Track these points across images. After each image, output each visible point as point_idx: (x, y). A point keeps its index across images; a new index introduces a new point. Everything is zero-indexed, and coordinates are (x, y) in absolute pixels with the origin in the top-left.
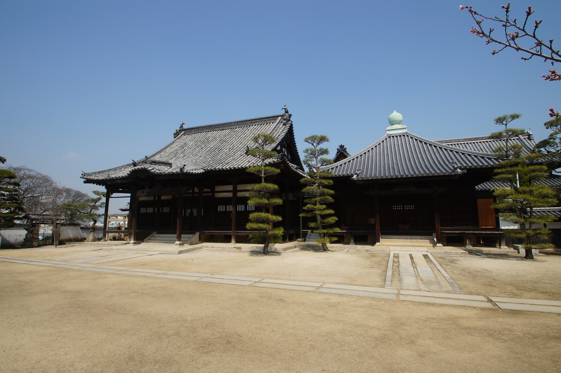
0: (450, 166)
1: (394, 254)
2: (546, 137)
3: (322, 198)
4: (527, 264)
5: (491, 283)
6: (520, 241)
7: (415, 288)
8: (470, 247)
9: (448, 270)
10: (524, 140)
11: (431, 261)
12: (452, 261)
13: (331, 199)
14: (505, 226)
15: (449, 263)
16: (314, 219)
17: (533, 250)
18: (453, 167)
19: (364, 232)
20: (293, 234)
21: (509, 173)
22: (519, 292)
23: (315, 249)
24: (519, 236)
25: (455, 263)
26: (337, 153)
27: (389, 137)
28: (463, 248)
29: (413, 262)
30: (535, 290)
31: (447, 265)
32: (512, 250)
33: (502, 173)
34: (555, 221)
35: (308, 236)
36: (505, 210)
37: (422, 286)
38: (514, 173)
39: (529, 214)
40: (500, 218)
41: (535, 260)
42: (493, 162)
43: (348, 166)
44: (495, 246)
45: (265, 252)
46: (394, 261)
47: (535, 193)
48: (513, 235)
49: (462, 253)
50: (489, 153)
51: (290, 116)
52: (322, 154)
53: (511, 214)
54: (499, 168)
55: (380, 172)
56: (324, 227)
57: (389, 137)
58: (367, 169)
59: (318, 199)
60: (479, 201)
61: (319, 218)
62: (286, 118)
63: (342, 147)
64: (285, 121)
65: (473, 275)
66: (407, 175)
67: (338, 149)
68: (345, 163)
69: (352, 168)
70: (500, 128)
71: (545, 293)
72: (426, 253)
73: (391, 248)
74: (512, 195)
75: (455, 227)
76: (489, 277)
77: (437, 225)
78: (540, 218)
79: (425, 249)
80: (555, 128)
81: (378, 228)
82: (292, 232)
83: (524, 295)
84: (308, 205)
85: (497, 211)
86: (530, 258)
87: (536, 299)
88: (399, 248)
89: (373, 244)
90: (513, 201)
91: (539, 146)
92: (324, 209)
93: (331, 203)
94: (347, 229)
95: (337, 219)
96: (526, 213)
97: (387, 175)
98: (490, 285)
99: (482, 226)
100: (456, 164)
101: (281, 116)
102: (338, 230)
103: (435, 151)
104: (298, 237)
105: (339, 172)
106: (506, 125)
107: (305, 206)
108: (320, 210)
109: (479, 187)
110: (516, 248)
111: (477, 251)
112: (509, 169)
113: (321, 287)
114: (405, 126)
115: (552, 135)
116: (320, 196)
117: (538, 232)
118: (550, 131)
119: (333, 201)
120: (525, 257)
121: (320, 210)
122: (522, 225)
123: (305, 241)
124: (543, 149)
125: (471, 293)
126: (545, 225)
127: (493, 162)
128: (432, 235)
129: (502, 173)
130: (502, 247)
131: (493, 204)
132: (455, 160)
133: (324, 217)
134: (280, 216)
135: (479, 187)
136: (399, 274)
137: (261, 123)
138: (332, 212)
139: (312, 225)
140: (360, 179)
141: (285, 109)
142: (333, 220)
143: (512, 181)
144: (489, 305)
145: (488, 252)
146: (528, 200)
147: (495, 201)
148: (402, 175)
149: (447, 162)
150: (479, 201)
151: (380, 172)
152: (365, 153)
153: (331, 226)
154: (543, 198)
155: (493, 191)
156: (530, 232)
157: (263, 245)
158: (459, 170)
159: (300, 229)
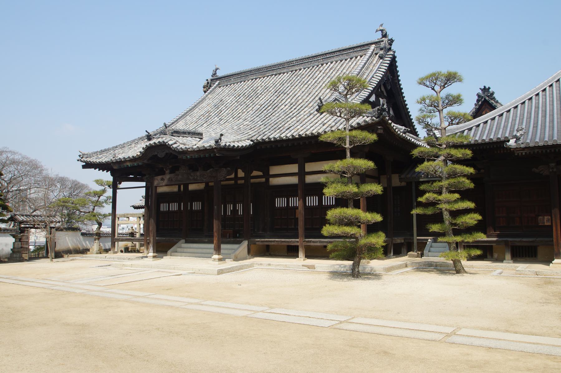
3: (452, 181)
13: (468, 184)
16: (438, 218)
19: (531, 239)
20: (402, 244)
23: (441, 269)
26: (478, 101)
35: (427, 247)
43: (499, 125)
45: (355, 274)
51: (391, 41)
52: (451, 105)
56: (457, 232)
58: (535, 127)
59: (445, 183)
61: (446, 216)
62: (385, 46)
63: (485, 90)
64: (382, 52)
67: (478, 95)
69: (505, 127)
84: (427, 195)
89: (548, 261)
92: (456, 201)
93: (469, 190)
94: (498, 236)
95: (480, 218)
101: (375, 43)
102: (481, 237)
108: (449, 202)
113: (454, 333)
119: (472, 186)
121: (449, 202)
123: (422, 255)
133: (455, 214)
134: (378, 213)
138: (470, 205)
140: (522, 146)
141: (382, 31)
142: (472, 219)
153: (469, 230)
157: (351, 263)
159: (413, 235)
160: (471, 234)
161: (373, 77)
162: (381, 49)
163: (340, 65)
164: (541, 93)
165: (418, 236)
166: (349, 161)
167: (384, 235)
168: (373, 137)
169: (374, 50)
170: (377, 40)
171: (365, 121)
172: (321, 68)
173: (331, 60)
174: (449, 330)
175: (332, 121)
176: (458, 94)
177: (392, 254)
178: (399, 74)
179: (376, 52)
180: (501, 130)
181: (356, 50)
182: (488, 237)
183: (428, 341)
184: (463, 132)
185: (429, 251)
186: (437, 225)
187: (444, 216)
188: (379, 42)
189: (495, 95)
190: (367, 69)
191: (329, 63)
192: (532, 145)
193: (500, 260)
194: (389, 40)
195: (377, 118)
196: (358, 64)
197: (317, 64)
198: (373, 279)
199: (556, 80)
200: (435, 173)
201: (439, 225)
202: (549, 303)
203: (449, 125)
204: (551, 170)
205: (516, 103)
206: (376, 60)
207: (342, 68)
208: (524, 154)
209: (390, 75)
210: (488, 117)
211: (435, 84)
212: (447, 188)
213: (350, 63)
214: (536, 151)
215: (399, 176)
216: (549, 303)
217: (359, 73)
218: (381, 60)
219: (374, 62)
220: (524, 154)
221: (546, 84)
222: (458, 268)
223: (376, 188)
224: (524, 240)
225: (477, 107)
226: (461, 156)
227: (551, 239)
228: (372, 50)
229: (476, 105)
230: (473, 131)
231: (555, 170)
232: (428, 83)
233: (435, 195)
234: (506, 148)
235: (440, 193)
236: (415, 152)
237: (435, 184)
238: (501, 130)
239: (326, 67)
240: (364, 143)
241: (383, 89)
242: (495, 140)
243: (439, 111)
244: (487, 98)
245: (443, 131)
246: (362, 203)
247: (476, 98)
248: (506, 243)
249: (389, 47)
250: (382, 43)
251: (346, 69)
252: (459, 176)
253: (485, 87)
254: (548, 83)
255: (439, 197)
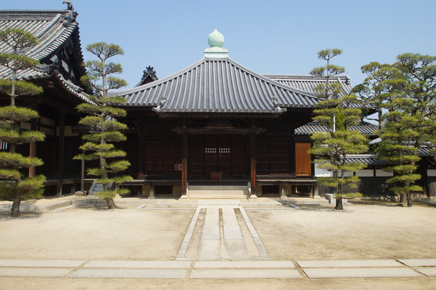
0: (271, 103)
1: (202, 209)
2: (361, 82)
3: (109, 133)
4: (338, 214)
5: (301, 241)
6: (332, 190)
7: (216, 257)
8: (284, 198)
9: (259, 228)
10: (342, 84)
11: (242, 217)
12: (264, 216)
13: (122, 137)
14: (320, 173)
15: (261, 219)
16: (96, 163)
17: (343, 200)
18: (274, 103)
19: (168, 181)
20: (71, 185)
21: (327, 114)
22: (328, 251)
23: (97, 205)
24: (332, 185)
25: (268, 218)
26: (144, 76)
27: (207, 62)
28: (278, 199)
29: (221, 219)
30: (343, 247)
31: (259, 221)
32: (324, 199)
33: (320, 114)
34: (365, 169)
35: (92, 188)
36: (320, 156)
37: (224, 254)
38: (331, 115)
39: (342, 161)
40: (316, 165)
41: (345, 211)
42: (313, 102)
43: (152, 93)
44: (308, 196)
45: (15, 213)
46: (198, 219)
47: (349, 138)
48: (326, 184)
49: (276, 205)
50: (309, 91)
51: (76, 15)
52: (113, 72)
53: (326, 160)
54: (318, 109)
55: (191, 103)
56: (111, 176)
57: (207, 62)
58: (176, 99)
59: (103, 135)
60: (297, 145)
61: (103, 162)
62: (70, 17)
63: (150, 69)
64: (66, 21)
65: (282, 232)
66: (223, 110)
67: (145, 72)
68: (148, 89)
69: (156, 96)
70: (322, 63)
71: (353, 250)
72: (237, 207)
73: (199, 202)
74: (328, 139)
75: (272, 175)
76: (299, 234)
77: (253, 172)
78: (352, 165)
79: (238, 202)
80: (370, 73)
81: (184, 175)
82: (68, 182)
83: (333, 255)
84: (87, 144)
85: (313, 157)
86: (339, 209)
87: (344, 259)
88: (209, 202)
89: (178, 197)
90: (329, 146)
91: (354, 91)
92: (111, 150)
93: (122, 142)
94: (146, 178)
95: (129, 164)
96: (339, 160)
97: (199, 108)
98: (301, 245)
99: (298, 174)
100: (277, 100)
101: (61, 13)
102: (129, 179)
103: (257, 84)
104: (79, 189)
105: (138, 100)
106: (328, 60)
107: (82, 145)
108: (105, 151)
109: (298, 131)
110: (328, 198)
111: (292, 202)
112: (327, 110)
113: (82, 267)
114: (226, 50)
115: (366, 80)
116: (105, 131)
117: (349, 180)
118: (366, 76)
119: (125, 138)
120: (336, 208)
121: (105, 151)
122: (335, 172)
123: (87, 194)
124: (357, 94)
125: (278, 258)
126: (354, 173)
127: (313, 102)
128: (247, 185)
129: (320, 114)
130: (315, 197)
131: (310, 150)
132: (276, 96)
133: (110, 160)
134: (39, 158)
135: (298, 131)
136: (200, 237)
137: (28, 18)
138: (122, 153)
139: (92, 172)
140: (165, 111)
141: (68, 3)
142: (124, 165)
143: (328, 124)
144: (296, 274)
145: (301, 203)
146: (342, 146)
147: (312, 145)
148: (217, 110)
149: (268, 98)
150: (297, 145)
151: (191, 103)
152: (176, 78)
153: (121, 174)
154: (355, 144)
155: (311, 135)
156: (342, 181)
157: (11, 203)
158: (279, 108)
159: (81, 177)
160: (122, 177)
161: (55, 40)
162: (66, 19)
163: (27, 24)
164: (183, 75)
165: (85, 178)
166: (13, 108)
167: (45, 177)
168: (39, 89)
169: (59, 18)
170: (63, 11)
171: (37, 75)
172: (8, 24)
173: (18, 19)
174: (77, 264)
175: (6, 71)
176: (118, 64)
177: (61, 193)
178: (80, 43)
179: (61, 20)
180: (153, 98)
181: (43, 14)
182: (135, 178)
183: (52, 279)
184: (125, 96)
185: (94, 191)
186: (94, 170)
187: (101, 162)
188: (65, 12)
189: (156, 74)
190: (51, 33)
191: (16, 21)
192: (171, 111)
193: (146, 196)
194: (74, 13)
195: (48, 74)
196: (43, 27)
197: (4, 19)
198: (32, 217)
199: (193, 68)
200: (95, 126)
201: (96, 169)
202: (169, 230)
203: (110, 88)
204: (183, 131)
205: (165, 79)
206: (60, 26)
207: (28, 27)
208: (165, 117)
209: (72, 42)
210: (145, 87)
211: (101, 53)
212: (105, 139)
213: (36, 25)
214: (174, 115)
215: (72, 128)
216: (169, 230)
217: (43, 34)
218: (65, 28)
219: (59, 28)
220: (165, 117)
221: (187, 70)
222: (110, 204)
223: (40, 136)
224: (163, 181)
225: (143, 81)
226: (117, 114)
227: (180, 181)
228: (57, 18)
229: (142, 79)
230: (132, 96)
231: (186, 131)
232: (95, 51)
233: (94, 145)
234: (153, 111)
235: (99, 143)
236: (80, 107)
237: (94, 135)
238: (153, 98)
239: (12, 24)
240: (30, 94)
241: (65, 53)
242: (147, 105)
243: (103, 75)
244: (150, 75)
245: (105, 92)
246: (32, 149)
247: (143, 74)
248: (151, 184)
249: (73, 18)
250: (67, 14)
251: (32, 29)
252: (114, 130)
253: (149, 66)
254: (188, 69)
255: (97, 146)
